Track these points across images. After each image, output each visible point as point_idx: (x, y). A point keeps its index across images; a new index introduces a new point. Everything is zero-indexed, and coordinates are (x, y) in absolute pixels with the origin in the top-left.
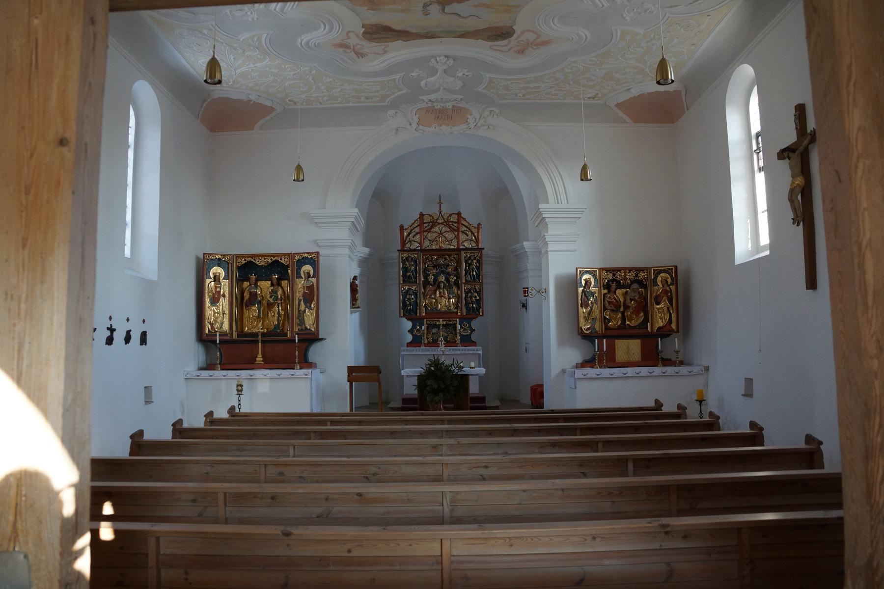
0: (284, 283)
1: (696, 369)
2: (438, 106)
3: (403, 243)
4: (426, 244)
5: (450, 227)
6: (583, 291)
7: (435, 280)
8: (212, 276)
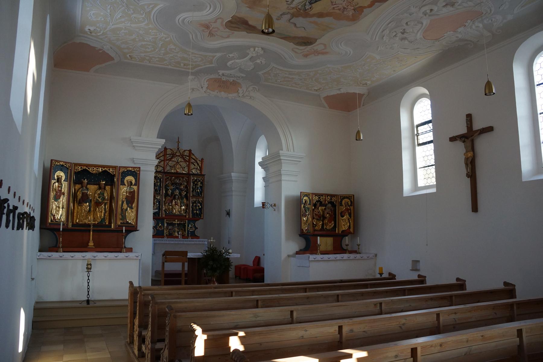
0: (108, 188)
1: (365, 256)
2: (224, 79)
4: (168, 169)
5: (184, 159)
6: (304, 207)
7: (172, 193)
8: (56, 178)
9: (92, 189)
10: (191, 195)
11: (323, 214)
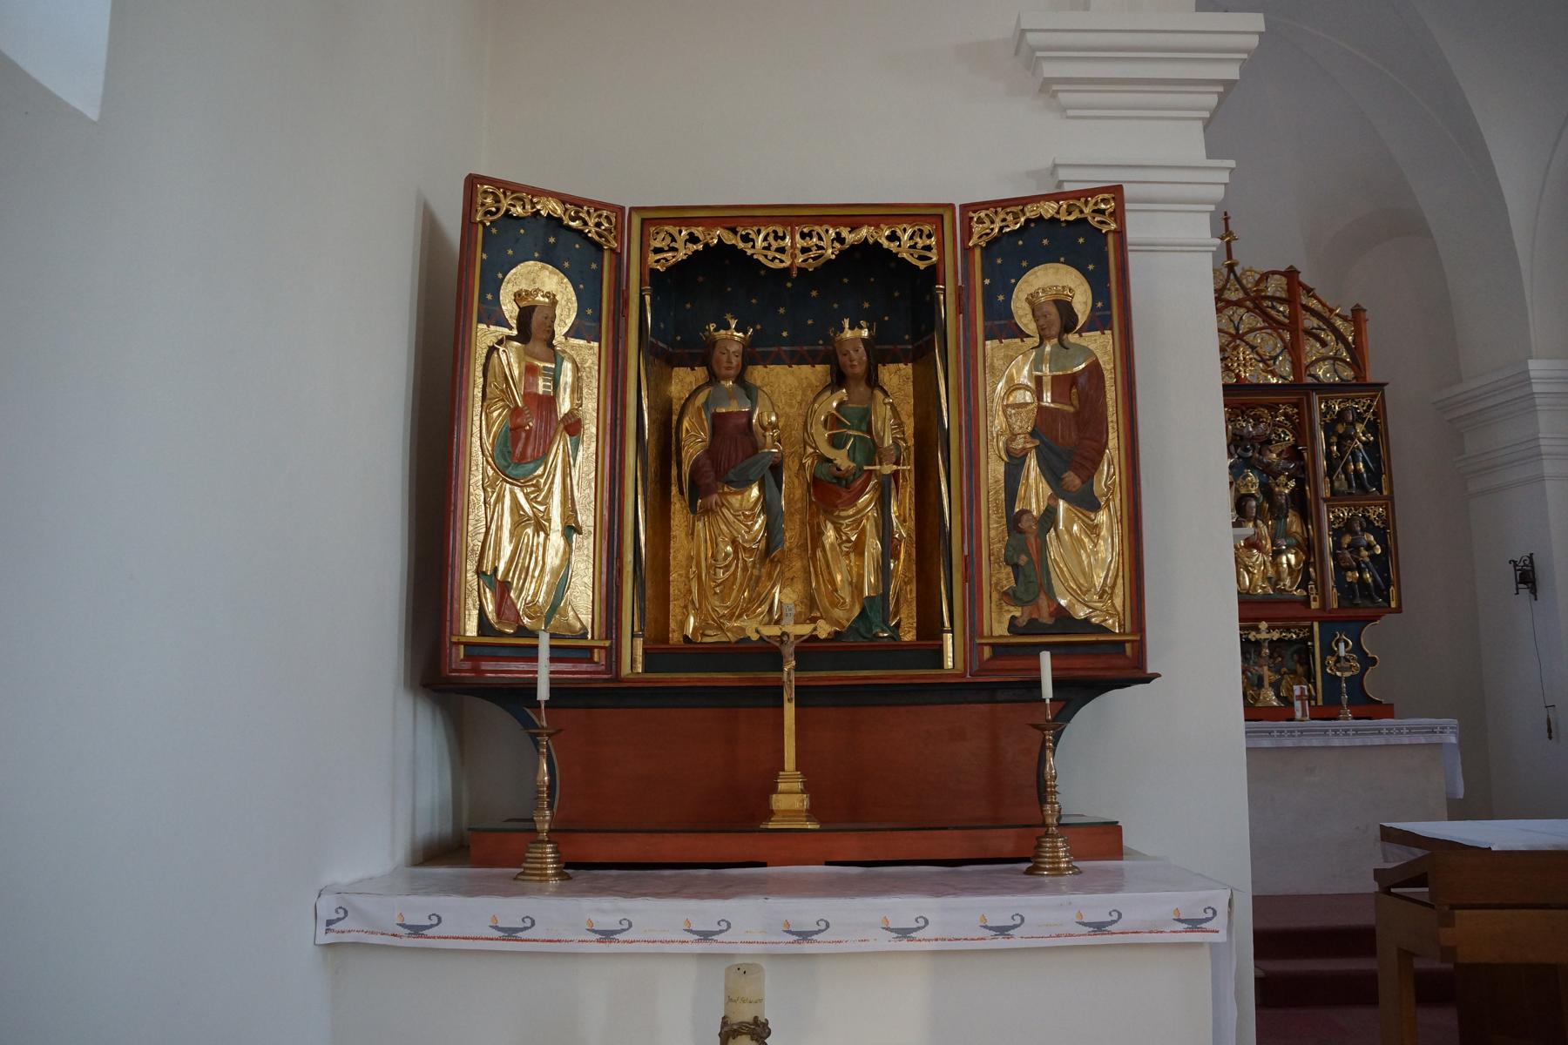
0: (897, 377)
8: (510, 309)
9: (786, 395)
10: (1325, 492)
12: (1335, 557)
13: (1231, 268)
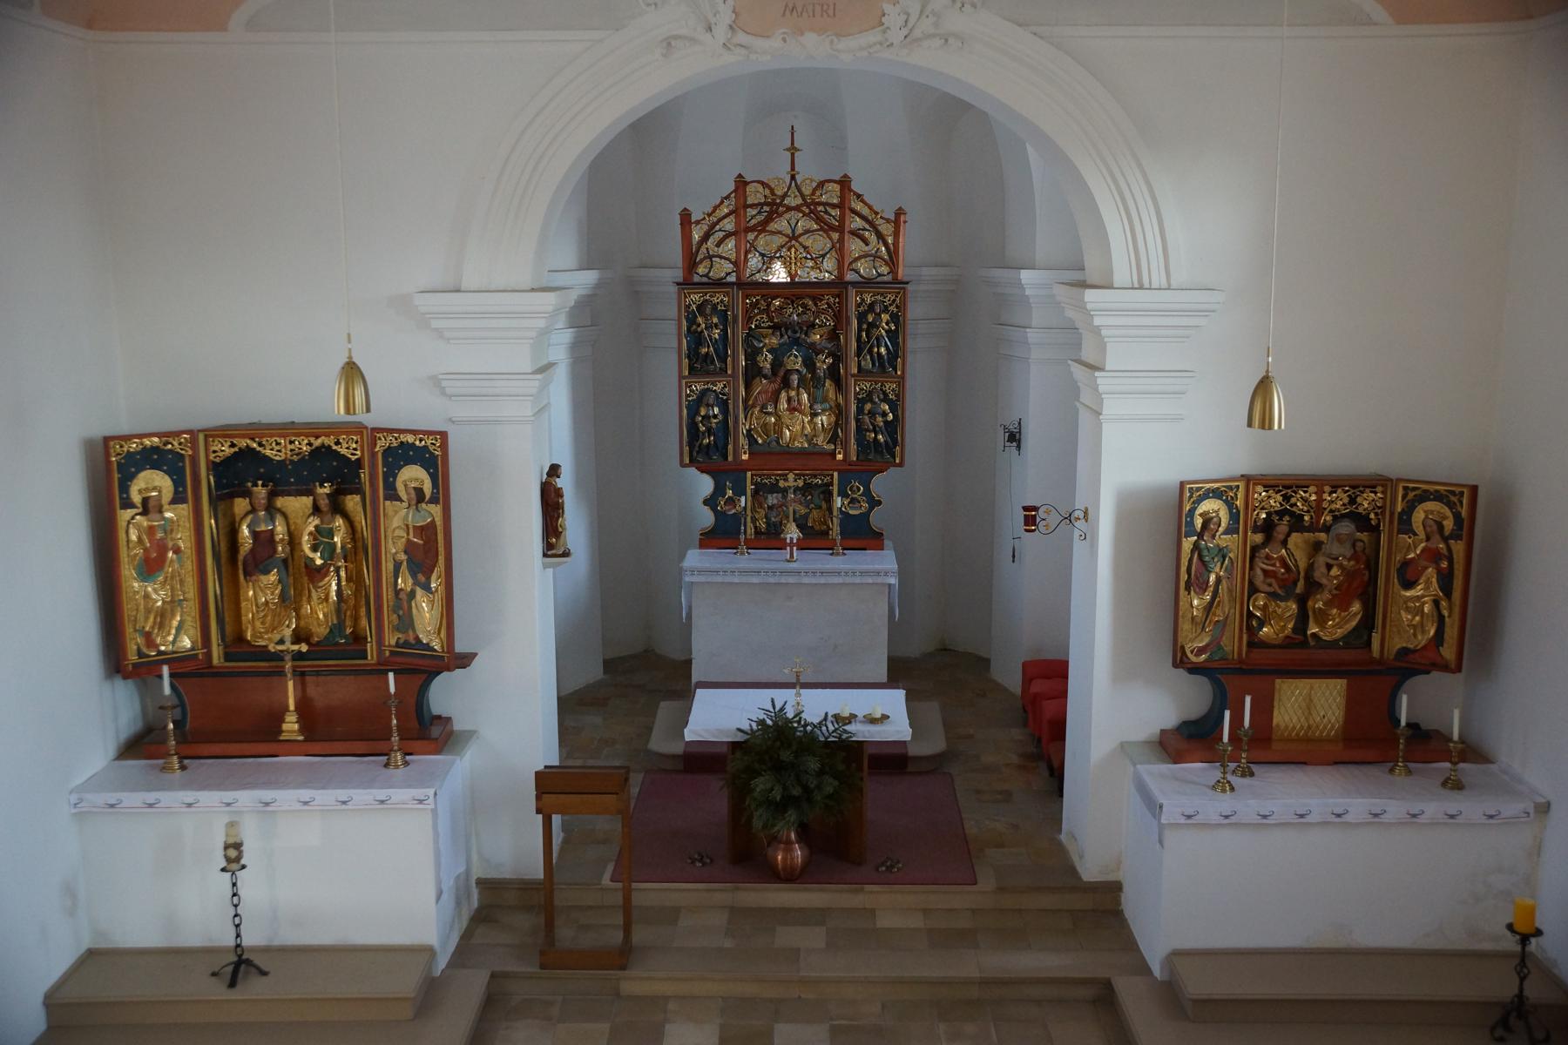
0: (352, 502)
3: (691, 263)
5: (819, 220)
6: (1196, 546)
7: (777, 364)
8: (136, 498)
10: (855, 371)
11: (1310, 568)
12: (857, 420)
13: (793, 178)
